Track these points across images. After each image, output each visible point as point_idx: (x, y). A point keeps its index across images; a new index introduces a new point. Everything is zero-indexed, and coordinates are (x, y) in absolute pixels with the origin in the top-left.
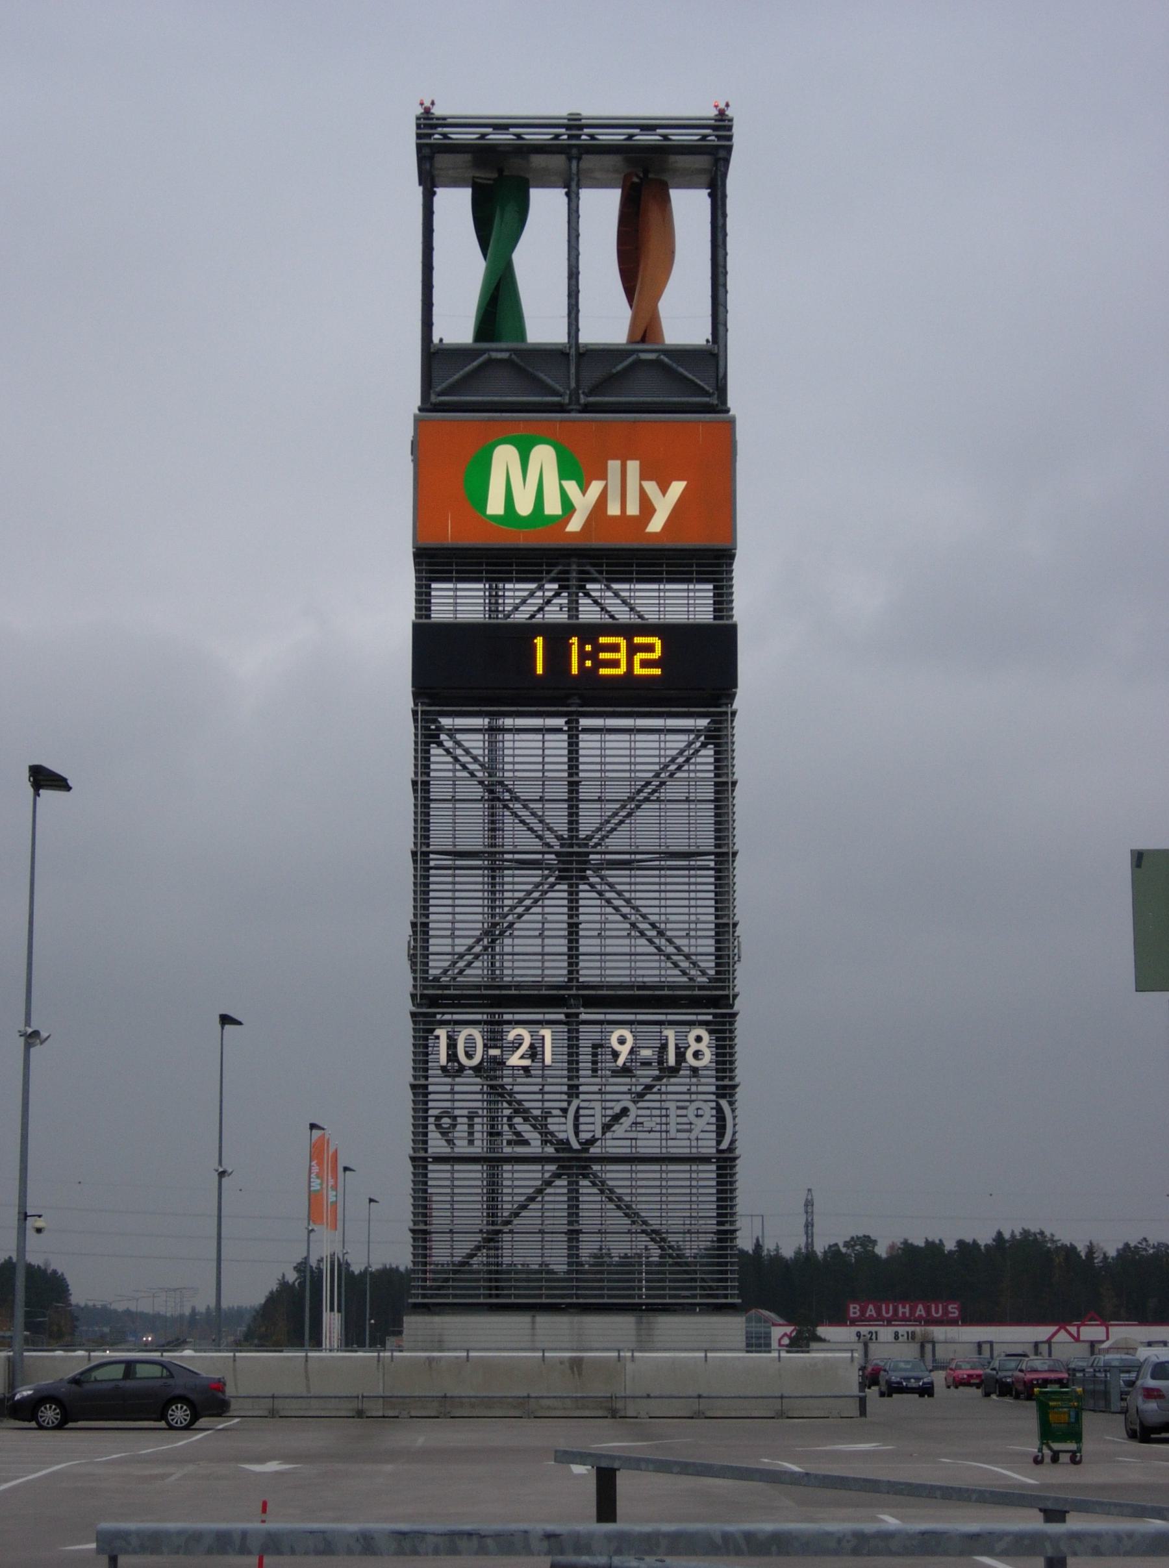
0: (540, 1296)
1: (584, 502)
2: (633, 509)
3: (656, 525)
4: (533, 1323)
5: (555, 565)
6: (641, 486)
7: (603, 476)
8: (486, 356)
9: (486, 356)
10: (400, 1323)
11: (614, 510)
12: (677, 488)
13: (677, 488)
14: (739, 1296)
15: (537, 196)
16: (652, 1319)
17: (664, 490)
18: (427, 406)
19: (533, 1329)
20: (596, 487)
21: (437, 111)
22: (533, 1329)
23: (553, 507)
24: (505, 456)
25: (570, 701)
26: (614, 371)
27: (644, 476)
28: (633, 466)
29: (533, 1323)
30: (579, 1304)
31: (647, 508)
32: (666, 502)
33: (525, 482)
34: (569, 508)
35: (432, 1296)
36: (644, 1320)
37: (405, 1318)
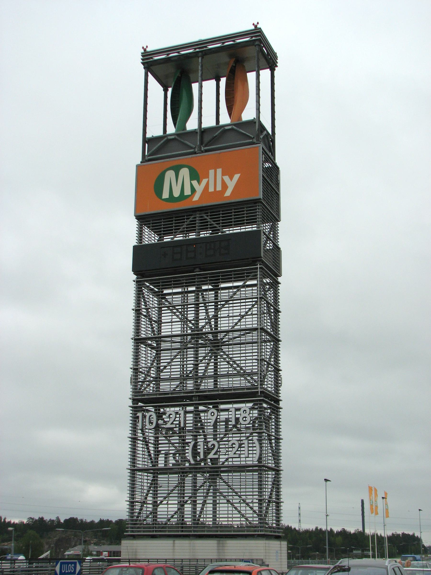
0: (217, 531)
1: (199, 188)
2: (219, 188)
3: (228, 193)
4: (174, 543)
5: (192, 215)
6: (222, 178)
7: (207, 177)
8: (166, 138)
9: (166, 138)
10: (121, 542)
11: (211, 189)
12: (237, 177)
13: (237, 177)
14: (283, 533)
15: (249, 75)
16: (224, 542)
17: (231, 179)
18: (144, 159)
19: (174, 546)
20: (204, 182)
21: (148, 50)
22: (174, 546)
23: (187, 192)
24: (170, 175)
25: (195, 271)
26: (215, 135)
27: (223, 174)
28: (219, 171)
29: (174, 543)
30: (196, 535)
31: (225, 186)
32: (231, 184)
33: (179, 184)
34: (193, 190)
35: (136, 531)
36: (221, 542)
37: (122, 541)
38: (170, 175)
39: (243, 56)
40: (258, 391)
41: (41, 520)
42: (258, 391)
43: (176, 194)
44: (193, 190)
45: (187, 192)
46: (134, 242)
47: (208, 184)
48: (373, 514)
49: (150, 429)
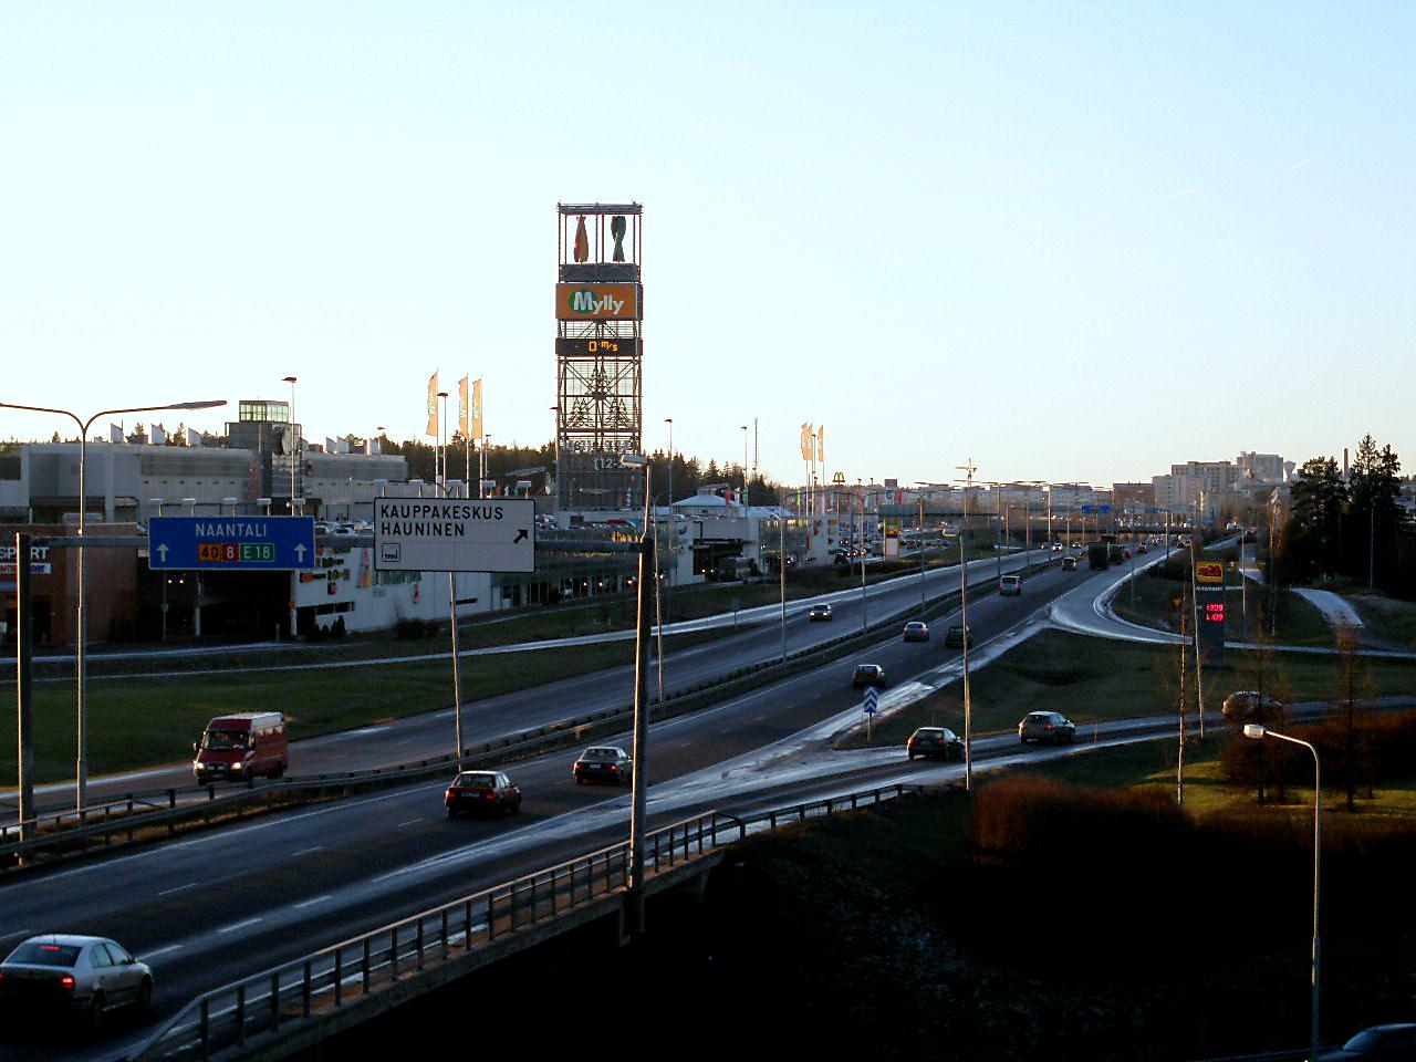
2: (610, 309)
12: (622, 302)
13: (622, 302)
23: (590, 308)
28: (611, 297)
31: (614, 308)
38: (578, 295)
39: (620, 216)
40: (460, 649)
41: (261, 436)
42: (460, 649)
43: (583, 308)
44: (594, 307)
45: (590, 308)
46: (556, 336)
47: (603, 306)
48: (808, 425)
49: (602, 523)
